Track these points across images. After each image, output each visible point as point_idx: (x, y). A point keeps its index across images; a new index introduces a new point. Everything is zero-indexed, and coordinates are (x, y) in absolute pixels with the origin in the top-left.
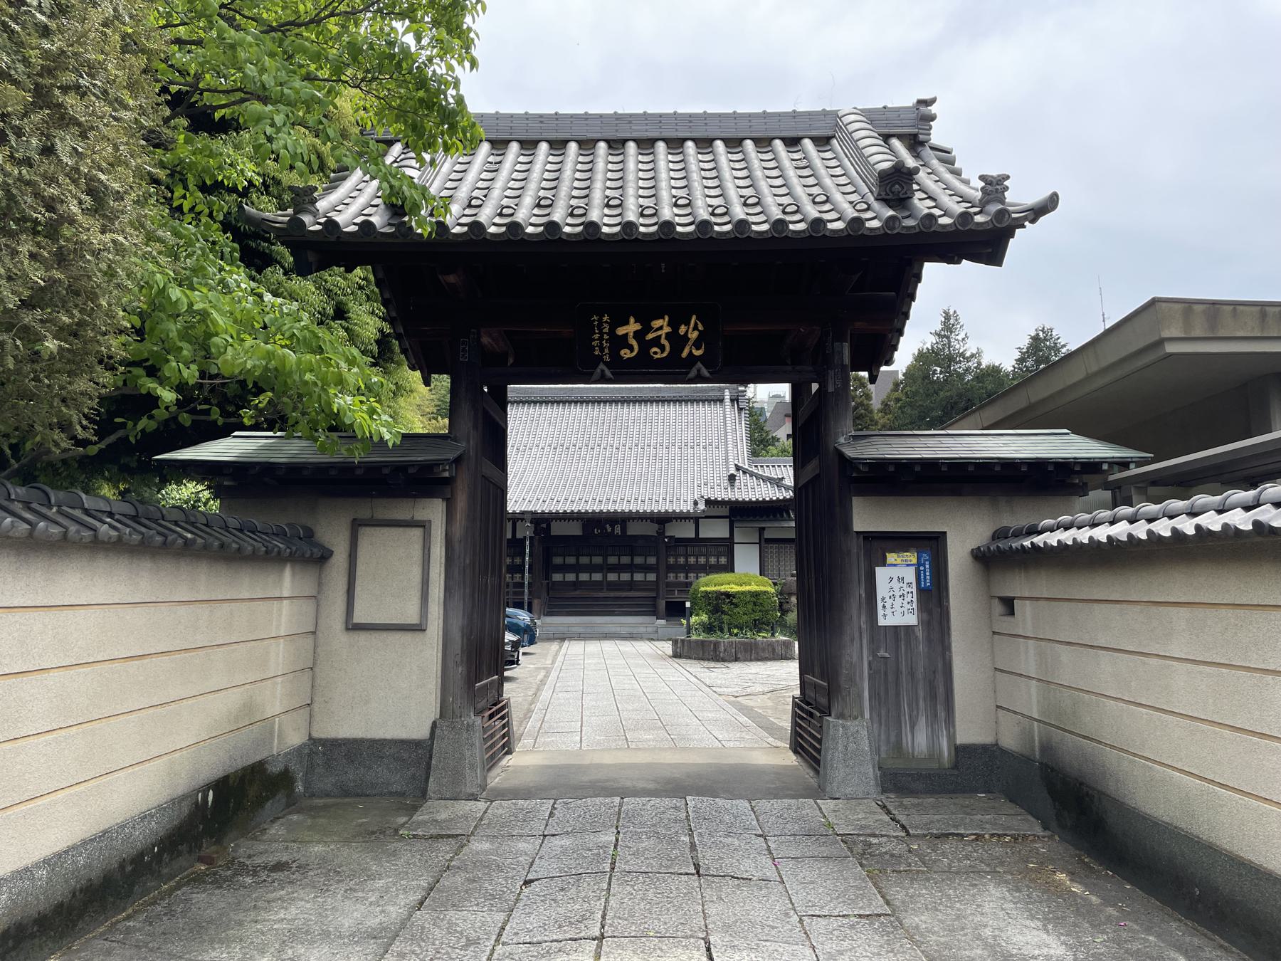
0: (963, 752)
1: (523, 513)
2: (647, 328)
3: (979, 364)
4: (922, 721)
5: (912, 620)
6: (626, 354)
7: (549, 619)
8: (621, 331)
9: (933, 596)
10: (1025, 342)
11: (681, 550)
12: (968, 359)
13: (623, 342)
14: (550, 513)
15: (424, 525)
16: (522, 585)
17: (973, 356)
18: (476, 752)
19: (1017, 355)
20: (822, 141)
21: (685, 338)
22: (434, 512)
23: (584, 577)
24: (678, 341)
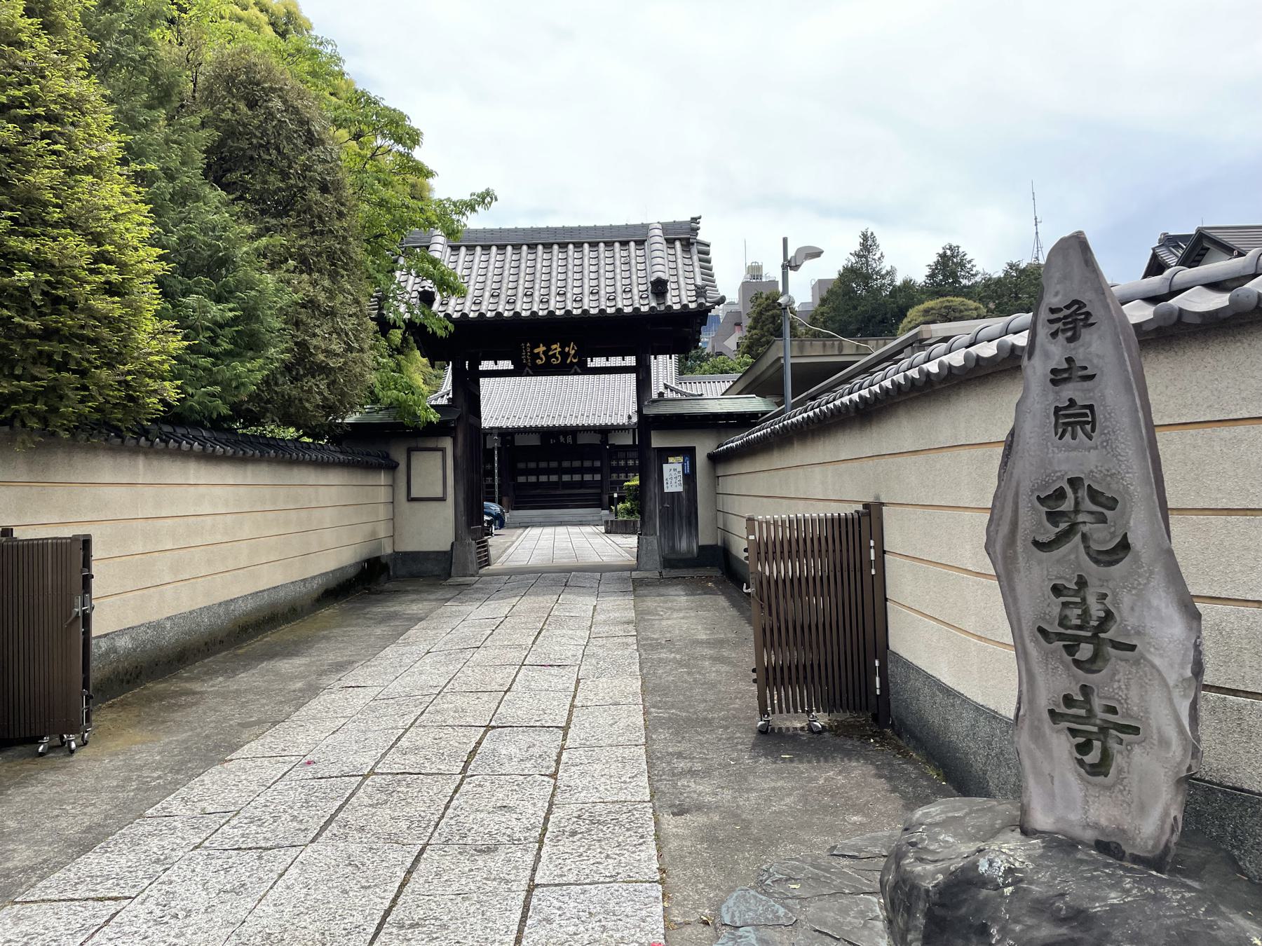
0: (702, 548)
1: (492, 428)
2: (549, 349)
3: (893, 281)
4: (685, 536)
5: (680, 489)
6: (539, 362)
7: (516, 513)
8: (536, 351)
9: (689, 478)
10: (933, 259)
11: (621, 455)
12: (883, 277)
13: (537, 356)
14: (513, 428)
15: (443, 450)
17: (888, 273)
18: (473, 557)
19: (927, 271)
20: (640, 243)
21: (568, 354)
22: (447, 443)
23: (543, 478)
24: (565, 355)
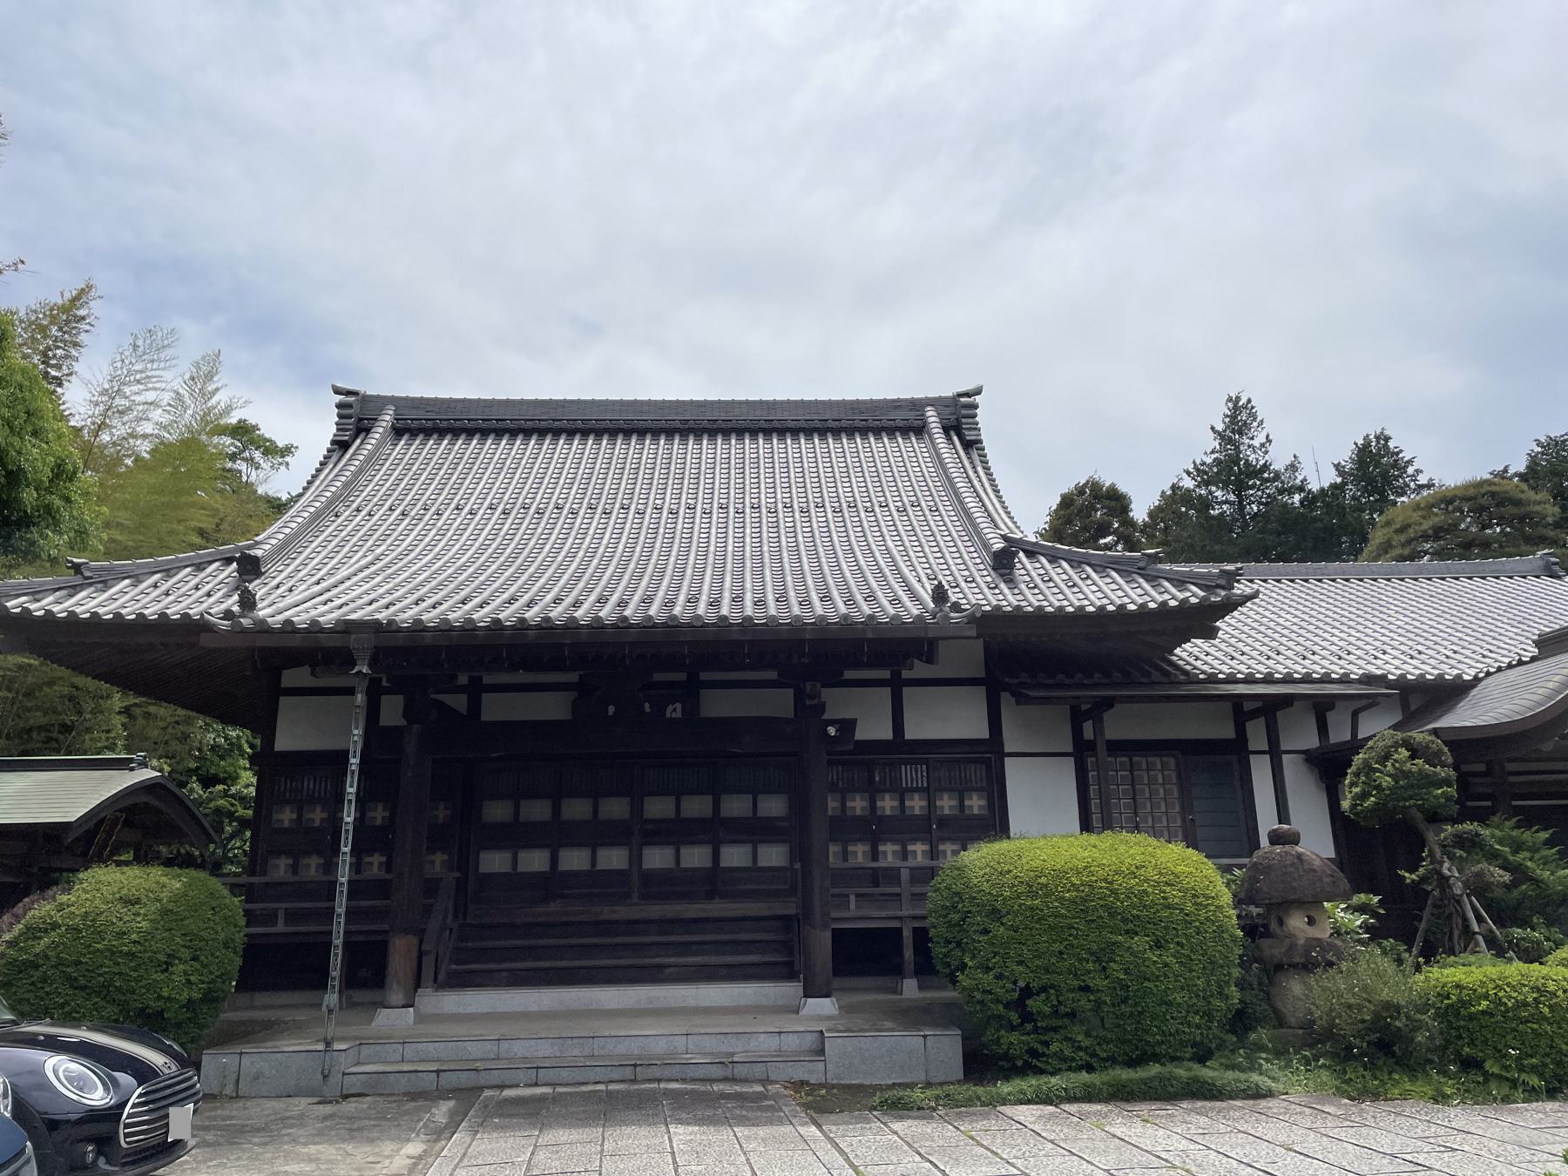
11: (910, 775)
16: (330, 890)
23: (574, 860)
